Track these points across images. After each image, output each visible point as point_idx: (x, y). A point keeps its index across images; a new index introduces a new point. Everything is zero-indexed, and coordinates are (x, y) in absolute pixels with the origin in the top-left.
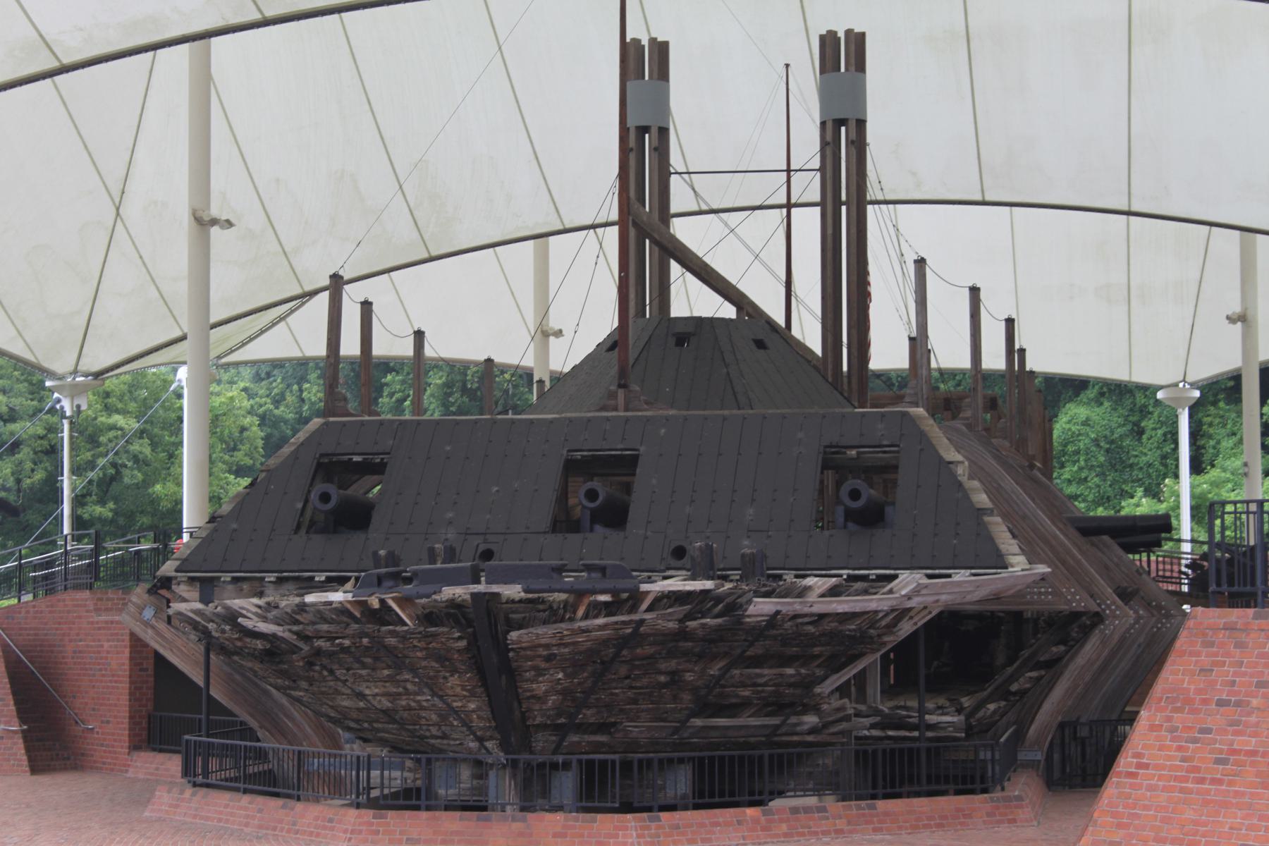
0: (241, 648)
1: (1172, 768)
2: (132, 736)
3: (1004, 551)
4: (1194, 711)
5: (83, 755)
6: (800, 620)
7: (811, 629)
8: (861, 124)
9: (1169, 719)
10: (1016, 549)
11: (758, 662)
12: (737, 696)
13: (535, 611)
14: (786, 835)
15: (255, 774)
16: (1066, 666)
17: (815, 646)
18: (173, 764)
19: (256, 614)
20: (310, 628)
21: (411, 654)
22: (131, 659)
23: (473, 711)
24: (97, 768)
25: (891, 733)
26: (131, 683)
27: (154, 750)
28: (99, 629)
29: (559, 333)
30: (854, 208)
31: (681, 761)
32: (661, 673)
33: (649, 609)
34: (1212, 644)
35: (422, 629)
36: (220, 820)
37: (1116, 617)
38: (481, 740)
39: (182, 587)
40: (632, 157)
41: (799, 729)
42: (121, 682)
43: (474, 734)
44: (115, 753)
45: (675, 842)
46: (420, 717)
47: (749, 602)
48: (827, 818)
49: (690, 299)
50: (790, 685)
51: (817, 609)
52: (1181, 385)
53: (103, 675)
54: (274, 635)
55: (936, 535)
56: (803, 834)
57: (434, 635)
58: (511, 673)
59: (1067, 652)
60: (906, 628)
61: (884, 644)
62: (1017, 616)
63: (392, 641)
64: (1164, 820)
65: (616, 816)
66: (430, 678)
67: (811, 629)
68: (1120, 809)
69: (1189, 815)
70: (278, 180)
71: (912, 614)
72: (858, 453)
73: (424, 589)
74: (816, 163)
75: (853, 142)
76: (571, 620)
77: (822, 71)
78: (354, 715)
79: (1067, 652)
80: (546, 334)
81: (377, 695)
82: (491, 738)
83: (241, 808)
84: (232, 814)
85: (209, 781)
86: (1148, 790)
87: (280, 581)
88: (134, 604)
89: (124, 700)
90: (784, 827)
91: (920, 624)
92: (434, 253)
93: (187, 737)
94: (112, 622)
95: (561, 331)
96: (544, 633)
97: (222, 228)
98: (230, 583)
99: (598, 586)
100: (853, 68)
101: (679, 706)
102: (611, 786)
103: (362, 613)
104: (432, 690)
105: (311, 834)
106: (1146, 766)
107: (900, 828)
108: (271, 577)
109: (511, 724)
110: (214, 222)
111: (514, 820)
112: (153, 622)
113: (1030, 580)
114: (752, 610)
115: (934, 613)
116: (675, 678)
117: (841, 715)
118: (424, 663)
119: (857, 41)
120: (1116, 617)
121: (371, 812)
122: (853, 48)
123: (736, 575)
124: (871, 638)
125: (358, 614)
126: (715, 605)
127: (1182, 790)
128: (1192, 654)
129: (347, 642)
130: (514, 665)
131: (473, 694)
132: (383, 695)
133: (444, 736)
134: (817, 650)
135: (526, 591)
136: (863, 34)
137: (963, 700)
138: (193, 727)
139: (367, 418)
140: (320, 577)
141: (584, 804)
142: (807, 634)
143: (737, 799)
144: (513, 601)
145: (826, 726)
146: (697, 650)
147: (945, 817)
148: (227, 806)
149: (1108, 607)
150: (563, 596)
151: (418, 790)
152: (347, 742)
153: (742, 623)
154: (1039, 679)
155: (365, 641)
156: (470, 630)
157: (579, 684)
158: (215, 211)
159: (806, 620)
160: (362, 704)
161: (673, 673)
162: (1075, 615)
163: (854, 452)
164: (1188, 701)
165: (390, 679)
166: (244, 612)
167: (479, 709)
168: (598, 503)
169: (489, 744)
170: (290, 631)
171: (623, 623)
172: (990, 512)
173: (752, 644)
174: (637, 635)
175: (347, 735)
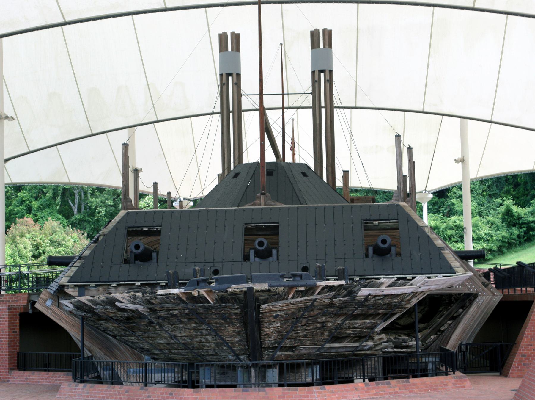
0: (112, 317)
6: (377, 298)
7: (380, 302)
8: (239, 75)
11: (356, 317)
12: (346, 333)
13: (271, 296)
16: (462, 318)
21: (210, 317)
23: (237, 342)
30: (329, 111)
32: (319, 323)
33: (319, 294)
35: (218, 304)
38: (237, 355)
41: (365, 348)
45: (338, 398)
47: (359, 290)
50: (366, 328)
52: (424, 192)
57: (224, 307)
58: (259, 323)
61: (405, 308)
62: (450, 295)
66: (217, 327)
72: (379, 223)
74: (310, 90)
75: (328, 81)
76: (287, 299)
77: (312, 49)
78: (162, 347)
80: (462, 160)
81: (184, 336)
82: (244, 354)
88: (42, 298)
90: (374, 391)
91: (420, 299)
92: (94, 132)
97: (9, 121)
98: (95, 287)
100: (327, 46)
103: (187, 299)
104: (216, 333)
108: (114, 284)
112: (52, 307)
114: (360, 293)
115: (426, 294)
119: (328, 34)
122: (327, 37)
125: (184, 299)
129: (176, 312)
131: (239, 334)
134: (380, 311)
136: (331, 31)
140: (138, 284)
144: (258, 291)
146: (335, 312)
151: (186, 381)
153: (355, 299)
154: (450, 325)
157: (286, 328)
159: (380, 298)
160: (172, 341)
161: (324, 323)
163: (377, 223)
166: (121, 300)
167: (240, 341)
168: (261, 248)
169: (242, 357)
170: (148, 308)
171: (308, 300)
173: (357, 309)
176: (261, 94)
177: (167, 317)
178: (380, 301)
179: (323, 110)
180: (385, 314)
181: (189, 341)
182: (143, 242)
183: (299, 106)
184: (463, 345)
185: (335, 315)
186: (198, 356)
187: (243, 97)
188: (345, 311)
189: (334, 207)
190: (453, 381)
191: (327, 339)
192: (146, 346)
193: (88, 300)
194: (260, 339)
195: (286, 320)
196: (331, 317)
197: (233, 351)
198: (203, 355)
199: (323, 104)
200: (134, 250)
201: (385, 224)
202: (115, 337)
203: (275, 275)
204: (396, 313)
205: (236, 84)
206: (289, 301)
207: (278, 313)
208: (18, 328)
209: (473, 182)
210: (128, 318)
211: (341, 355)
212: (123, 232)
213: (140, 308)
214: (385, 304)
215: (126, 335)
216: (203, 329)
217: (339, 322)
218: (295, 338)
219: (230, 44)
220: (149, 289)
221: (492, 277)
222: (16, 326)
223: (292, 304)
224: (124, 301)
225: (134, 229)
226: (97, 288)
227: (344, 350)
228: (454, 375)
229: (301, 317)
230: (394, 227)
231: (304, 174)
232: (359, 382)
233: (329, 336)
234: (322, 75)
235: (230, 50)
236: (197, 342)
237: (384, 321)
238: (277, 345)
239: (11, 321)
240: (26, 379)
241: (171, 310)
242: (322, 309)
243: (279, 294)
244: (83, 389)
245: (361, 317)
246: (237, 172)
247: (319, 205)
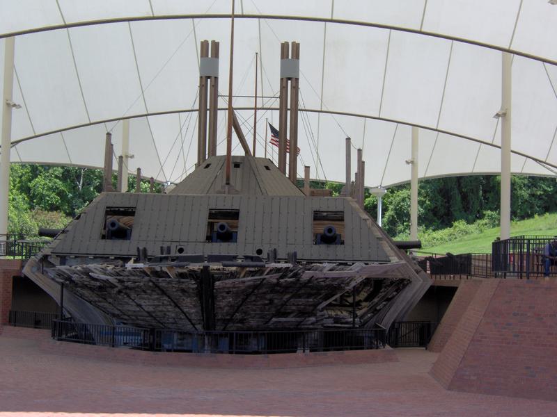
0: (86, 285)
7: (323, 283)
8: (216, 78)
10: (393, 254)
32: (266, 299)
38: (193, 325)
40: (203, 88)
55: (370, 247)
57: (183, 282)
58: (213, 297)
63: (164, 284)
67: (323, 283)
74: (278, 95)
76: (238, 278)
78: (130, 313)
80: (412, 162)
96: (229, 282)
103: (151, 272)
106: (485, 338)
116: (271, 301)
118: (175, 293)
119: (296, 47)
125: (149, 273)
129: (142, 284)
130: (215, 295)
131: (195, 306)
133: (175, 323)
136: (218, 43)
154: (385, 305)
155: (151, 284)
163: (325, 214)
166: (94, 270)
167: (197, 312)
168: (220, 231)
176: (230, 96)
179: (289, 112)
187: (219, 98)
192: (117, 312)
197: (190, 320)
199: (289, 107)
200: (111, 228)
202: (90, 302)
205: (294, 87)
206: (241, 280)
207: (231, 289)
209: (420, 181)
210: (100, 287)
213: (112, 279)
215: (100, 302)
219: (209, 52)
220: (121, 262)
221: (428, 264)
231: (267, 168)
232: (300, 353)
234: (290, 81)
235: (290, 57)
236: (160, 311)
241: (312, 263)
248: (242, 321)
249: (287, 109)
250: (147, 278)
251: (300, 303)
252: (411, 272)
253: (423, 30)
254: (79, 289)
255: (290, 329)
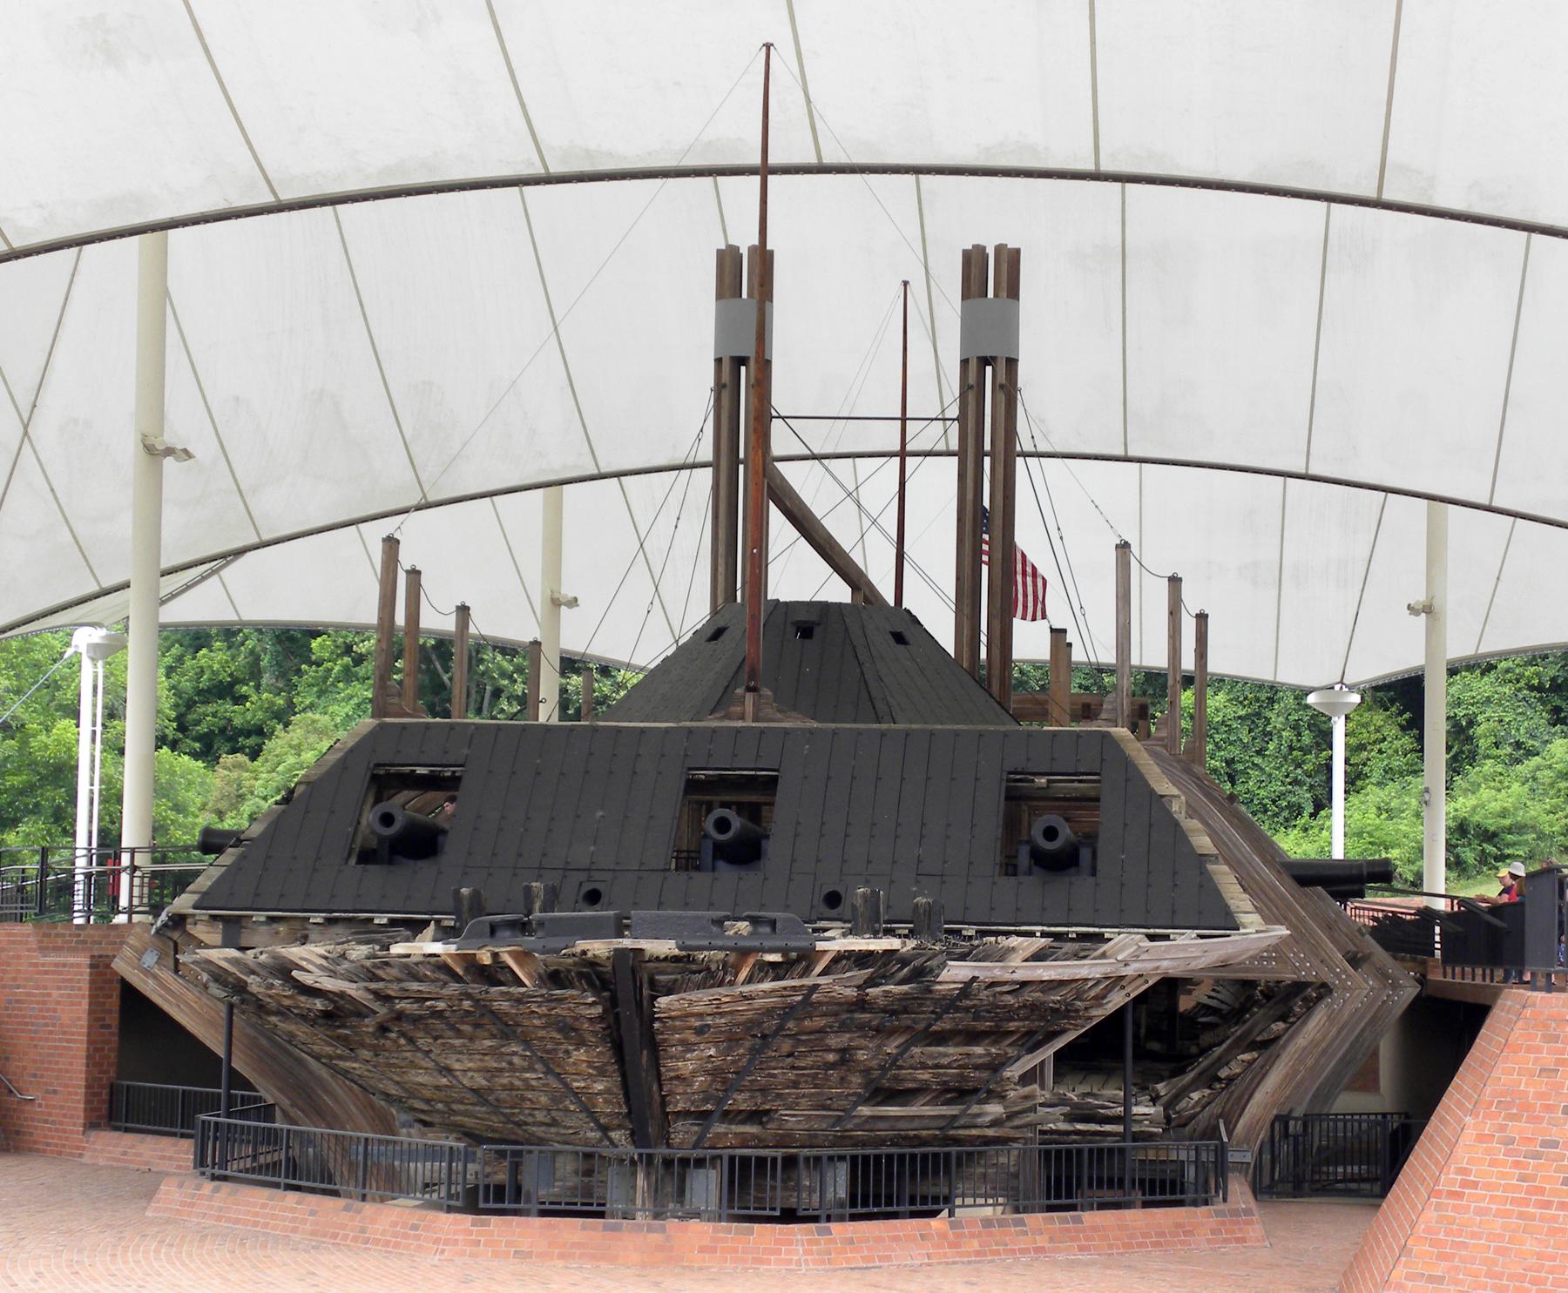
0: (288, 1008)
1: (1506, 1188)
2: (90, 1109)
3: (1233, 908)
4: (1537, 1120)
5: (18, 1133)
7: (1010, 999)
8: (1012, 363)
9: (1502, 1128)
10: (1250, 907)
11: (941, 1038)
12: (915, 1080)
14: (978, 1253)
15: (268, 1165)
16: (1284, 1047)
17: (1013, 1020)
18: (181, 1151)
19: (321, 967)
20: (395, 986)
22: (90, 1012)
23: (600, 1093)
24: (37, 1150)
25: (1079, 1126)
26: (90, 1042)
27: (117, 1129)
28: (46, 973)
29: (573, 602)
31: (842, 1158)
32: (829, 1050)
34: (1555, 1039)
36: (256, 1224)
37: (1346, 989)
38: (605, 1129)
39: (200, 927)
42: (75, 1041)
43: (597, 1122)
44: (65, 1131)
46: (523, 1099)
47: (943, 965)
48: (1025, 1233)
49: (797, 576)
50: (976, 1067)
51: (1020, 975)
52: (1337, 687)
53: (51, 1032)
54: (342, 995)
56: (997, 1253)
57: (560, 1000)
58: (655, 1048)
59: (1287, 1030)
60: (1116, 1000)
61: (1090, 1018)
63: (505, 1006)
64: (1498, 1251)
65: (779, 1226)
66: (548, 1052)
67: (1010, 999)
68: (1441, 1236)
69: (1530, 1245)
70: (237, 399)
71: (1123, 983)
73: (553, 943)
75: (1002, 386)
76: (731, 983)
78: (427, 1093)
79: (1287, 1030)
80: (556, 603)
81: (470, 1070)
82: (620, 1127)
83: (284, 1209)
84: (273, 1217)
85: (228, 1173)
86: (1476, 1213)
87: (330, 922)
88: (131, 946)
89: (80, 1065)
90: (975, 1244)
93: (203, 1117)
94: (64, 965)
95: (576, 599)
96: (700, 999)
97: (177, 460)
99: (767, 944)
101: (846, 1091)
102: (762, 1191)
103: (467, 970)
104: (546, 1066)
105: (387, 1243)
106: (1475, 1185)
107: (1110, 1246)
108: (317, 918)
109: (644, 1109)
110: (169, 451)
111: (650, 1229)
113: (1264, 944)
114: (945, 975)
116: (845, 1055)
117: (1029, 1104)
118: (541, 1033)
119: (1010, 260)
120: (1346, 989)
121: (470, 1217)
122: (1005, 267)
123: (903, 928)
124: (1077, 1011)
126: (901, 969)
127: (1521, 1216)
128: (1529, 1050)
129: (441, 1005)
131: (602, 1072)
132: (478, 1070)
133: (554, 1123)
134: (1012, 1026)
135: (680, 949)
136: (1018, 251)
137: (1159, 1086)
138: (211, 1104)
139: (430, 720)
140: (381, 919)
141: (736, 1211)
142: (1005, 1006)
143: (895, 1208)
144: (657, 959)
145: (1011, 1116)
146: (875, 1023)
147: (1163, 1234)
148: (264, 1206)
149: (1337, 975)
150: (721, 955)
152: (404, 1126)
153: (931, 992)
154: (1251, 1063)
155: (467, 1004)
156: (606, 994)
157: (733, 1062)
158: (169, 439)
159: (1006, 988)
160: (444, 1081)
161: (842, 1051)
162: (1299, 987)
164: (1527, 1107)
165: (492, 1052)
166: (304, 964)
167: (608, 1091)
168: (730, 834)
169: (614, 1135)
170: (367, 989)
172: (1214, 859)
173: (939, 1017)
174: (807, 1004)
175: (404, 1117)
177: (421, 1017)
178: (1008, 997)
180: (1030, 1033)
181: (484, 1083)
182: (406, 806)
183: (928, 448)
184: (1296, 1119)
185: (878, 1030)
186: (515, 1123)
188: (906, 1020)
189: (932, 733)
190: (1213, 1222)
191: (859, 1095)
193: (226, 960)
194: (661, 1089)
195: (732, 1040)
196: (865, 1036)
197: (592, 1115)
198: (526, 1124)
201: (1066, 787)
203: (698, 918)
204: (1063, 1032)
208: (116, 1015)
210: (327, 1015)
211: (906, 1138)
212: (359, 779)
214: (1025, 1006)
215: (340, 1058)
216: (515, 1053)
217: (891, 1048)
218: (763, 1090)
219: (991, 278)
222: (110, 1012)
223: (746, 998)
224: (310, 967)
225: (393, 770)
226: (274, 926)
227: (916, 1124)
228: (1221, 1207)
229: (776, 1033)
230: (1092, 794)
231: (899, 638)
233: (865, 1086)
235: (991, 294)
236: (504, 1088)
237: (1031, 1050)
238: (709, 1107)
239: (97, 996)
240: (125, 1153)
242: (836, 1014)
243: (708, 969)
244: (210, 1198)
245: (958, 1039)
246: (722, 624)
247: (914, 726)
248: (756, 1116)
249: (737, 462)
250: (453, 988)
251: (945, 1061)
252: (1328, 963)
253: (1388, 196)
254: (274, 1019)
255: (924, 1142)
